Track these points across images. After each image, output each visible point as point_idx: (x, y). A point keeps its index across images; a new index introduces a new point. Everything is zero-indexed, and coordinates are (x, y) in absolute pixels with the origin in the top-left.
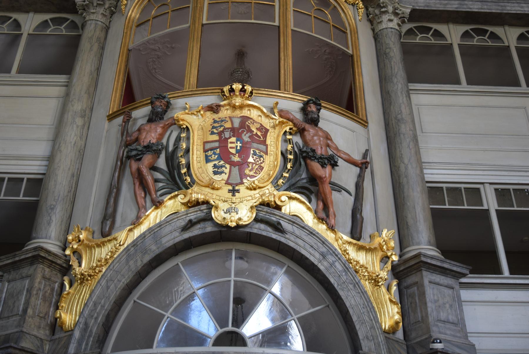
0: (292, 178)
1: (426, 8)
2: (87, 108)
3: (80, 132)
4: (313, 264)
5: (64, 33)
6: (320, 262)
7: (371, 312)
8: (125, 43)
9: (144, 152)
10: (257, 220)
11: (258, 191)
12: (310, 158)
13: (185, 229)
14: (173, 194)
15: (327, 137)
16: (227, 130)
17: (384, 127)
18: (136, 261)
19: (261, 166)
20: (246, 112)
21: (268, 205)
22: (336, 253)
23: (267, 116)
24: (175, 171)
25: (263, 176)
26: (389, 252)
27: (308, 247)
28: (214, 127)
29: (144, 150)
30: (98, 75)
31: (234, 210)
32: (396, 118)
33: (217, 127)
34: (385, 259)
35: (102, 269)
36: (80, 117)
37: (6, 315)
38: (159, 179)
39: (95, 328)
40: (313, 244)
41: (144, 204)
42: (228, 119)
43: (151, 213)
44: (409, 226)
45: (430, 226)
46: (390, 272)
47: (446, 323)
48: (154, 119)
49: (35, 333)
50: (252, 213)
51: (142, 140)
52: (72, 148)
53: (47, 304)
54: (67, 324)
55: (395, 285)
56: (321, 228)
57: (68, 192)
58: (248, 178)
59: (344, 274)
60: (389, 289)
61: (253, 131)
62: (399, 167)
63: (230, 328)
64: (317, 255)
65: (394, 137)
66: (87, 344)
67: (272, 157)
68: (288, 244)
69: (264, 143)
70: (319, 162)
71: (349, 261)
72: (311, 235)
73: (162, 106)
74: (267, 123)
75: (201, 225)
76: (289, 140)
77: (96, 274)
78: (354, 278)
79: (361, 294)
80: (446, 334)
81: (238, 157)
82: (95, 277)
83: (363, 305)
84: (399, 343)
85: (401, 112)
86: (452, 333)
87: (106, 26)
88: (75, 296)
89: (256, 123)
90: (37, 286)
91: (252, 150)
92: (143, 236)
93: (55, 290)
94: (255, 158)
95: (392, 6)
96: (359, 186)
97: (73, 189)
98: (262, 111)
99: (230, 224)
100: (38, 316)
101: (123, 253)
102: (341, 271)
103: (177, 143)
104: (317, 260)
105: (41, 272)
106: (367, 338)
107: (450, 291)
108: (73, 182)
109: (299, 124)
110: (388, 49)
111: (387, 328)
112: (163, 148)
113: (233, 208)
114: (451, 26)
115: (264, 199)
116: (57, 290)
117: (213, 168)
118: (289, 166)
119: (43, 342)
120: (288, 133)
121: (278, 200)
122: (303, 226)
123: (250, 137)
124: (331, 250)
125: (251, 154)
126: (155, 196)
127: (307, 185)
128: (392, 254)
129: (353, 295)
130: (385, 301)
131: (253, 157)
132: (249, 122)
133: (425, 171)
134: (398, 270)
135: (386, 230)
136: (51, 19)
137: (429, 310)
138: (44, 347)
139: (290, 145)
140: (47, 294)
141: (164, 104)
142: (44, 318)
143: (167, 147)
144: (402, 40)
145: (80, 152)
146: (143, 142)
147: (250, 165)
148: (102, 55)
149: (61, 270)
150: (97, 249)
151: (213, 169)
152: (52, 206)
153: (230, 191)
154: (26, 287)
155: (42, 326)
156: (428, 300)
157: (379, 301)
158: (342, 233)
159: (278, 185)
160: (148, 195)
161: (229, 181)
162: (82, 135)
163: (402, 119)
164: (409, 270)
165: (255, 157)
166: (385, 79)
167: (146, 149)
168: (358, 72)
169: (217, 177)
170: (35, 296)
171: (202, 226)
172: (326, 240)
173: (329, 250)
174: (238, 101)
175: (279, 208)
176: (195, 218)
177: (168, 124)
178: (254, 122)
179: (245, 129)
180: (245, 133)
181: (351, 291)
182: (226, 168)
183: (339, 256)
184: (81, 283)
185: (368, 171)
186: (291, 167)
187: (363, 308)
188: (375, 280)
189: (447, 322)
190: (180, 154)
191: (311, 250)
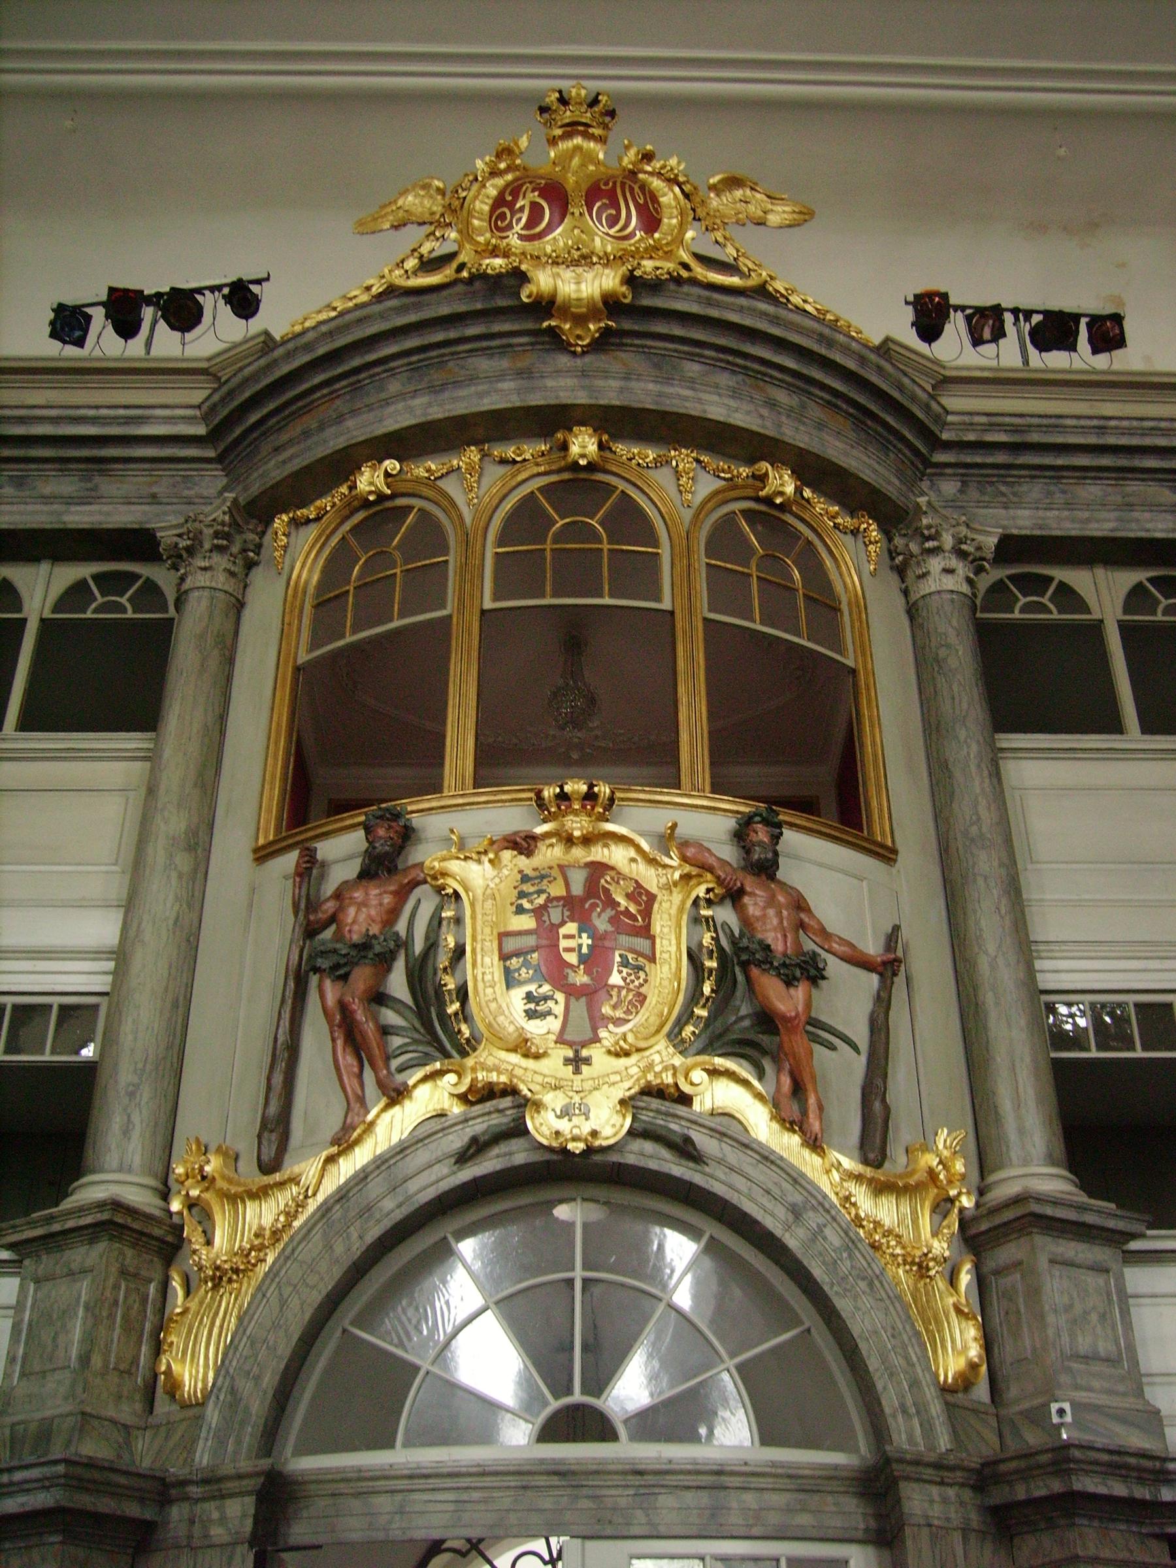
0: (715, 1018)
1: (1038, 532)
3: (187, 888)
4: (771, 1235)
5: (130, 614)
6: (788, 1228)
8: (288, 654)
9: (356, 960)
10: (631, 1133)
11: (634, 1058)
12: (758, 964)
13: (463, 1157)
14: (428, 1069)
15: (800, 905)
16: (555, 903)
17: (936, 854)
18: (348, 1237)
19: (639, 994)
20: (599, 853)
22: (827, 1206)
23: (652, 862)
24: (433, 1009)
27: (758, 1193)
29: (354, 953)
30: (222, 733)
32: (966, 833)
33: (531, 894)
34: (943, 1206)
35: (266, 1254)
36: (186, 849)
37: (37, 1368)
38: (392, 1027)
39: (257, 1405)
40: (771, 1186)
41: (360, 1092)
42: (555, 872)
43: (378, 1116)
46: (955, 1239)
49: (111, 1412)
50: (624, 1116)
51: (347, 928)
54: (187, 1389)
55: (968, 1272)
56: (788, 1145)
58: (611, 1026)
59: (845, 1255)
60: (953, 1281)
61: (619, 904)
63: (577, 1397)
64: (781, 1212)
65: (963, 884)
66: (239, 1442)
67: (666, 968)
68: (711, 1189)
69: (645, 932)
70: (779, 975)
71: (858, 1221)
73: (391, 839)
74: (650, 878)
76: (707, 919)
79: (888, 1302)
80: (1089, 1389)
82: (250, 1274)
83: (893, 1328)
85: (979, 819)
86: (1106, 1385)
87: (238, 600)
88: (202, 1318)
92: (362, 1177)
94: (624, 974)
95: (951, 532)
96: (879, 1027)
97: (177, 1041)
99: (570, 1146)
100: (114, 1369)
101: (317, 1217)
103: (432, 935)
106: (905, 1411)
107: (1100, 1280)
110: (944, 649)
111: (950, 1380)
112: (398, 946)
114: (1100, 572)
116: (154, 1300)
118: (707, 989)
119: (129, 1433)
120: (702, 903)
121: (683, 1080)
122: (746, 1141)
123: (613, 920)
126: (385, 1072)
127: (751, 1036)
128: (960, 1194)
131: (620, 972)
132: (608, 879)
133: (1038, 964)
134: (973, 1231)
135: (945, 1131)
136: (97, 578)
140: (133, 1313)
141: (396, 832)
142: (129, 1373)
143: (405, 944)
144: (979, 615)
145: (188, 941)
146: (350, 931)
147: (614, 993)
148: (229, 679)
150: (248, 1203)
154: (83, 1298)
155: (125, 1393)
157: (930, 1313)
159: (683, 1041)
161: (567, 1037)
165: (625, 970)
166: (938, 730)
168: (870, 717)
169: (535, 1028)
170: (105, 1321)
172: (803, 1175)
174: (577, 825)
175: (685, 1100)
176: (484, 1133)
178: (619, 876)
179: (599, 898)
183: (833, 1213)
184: (215, 1287)
185: (900, 980)
186: (713, 991)
188: (920, 1265)
189: (1093, 1359)
190: (443, 961)
191: (765, 1200)
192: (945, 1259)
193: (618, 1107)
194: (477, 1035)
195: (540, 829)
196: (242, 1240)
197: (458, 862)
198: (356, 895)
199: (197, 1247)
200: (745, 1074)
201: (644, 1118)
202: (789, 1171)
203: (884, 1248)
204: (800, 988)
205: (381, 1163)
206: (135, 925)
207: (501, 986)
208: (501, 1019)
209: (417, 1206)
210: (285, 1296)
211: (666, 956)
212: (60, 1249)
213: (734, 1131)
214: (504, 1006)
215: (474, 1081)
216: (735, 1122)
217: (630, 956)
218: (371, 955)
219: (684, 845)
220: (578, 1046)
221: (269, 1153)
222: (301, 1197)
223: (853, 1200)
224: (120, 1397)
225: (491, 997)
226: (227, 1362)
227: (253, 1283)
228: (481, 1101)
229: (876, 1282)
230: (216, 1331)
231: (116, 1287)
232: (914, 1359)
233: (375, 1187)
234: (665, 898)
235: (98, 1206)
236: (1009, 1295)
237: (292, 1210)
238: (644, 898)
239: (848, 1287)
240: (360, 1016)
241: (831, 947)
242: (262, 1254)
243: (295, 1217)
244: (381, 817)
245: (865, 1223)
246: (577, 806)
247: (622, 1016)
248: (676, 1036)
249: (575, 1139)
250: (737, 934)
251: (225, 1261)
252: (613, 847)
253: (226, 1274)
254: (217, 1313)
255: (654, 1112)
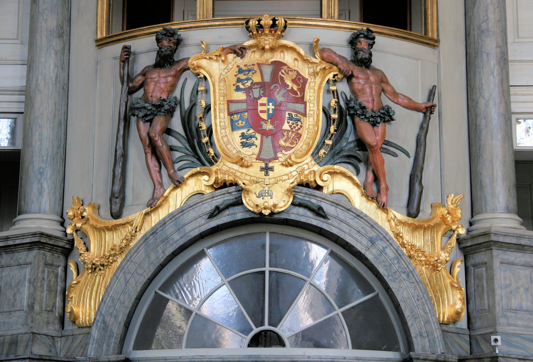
2: (64, 21)
7: (427, 304)
9: (155, 113)
10: (293, 204)
11: (295, 167)
12: (359, 116)
13: (212, 215)
15: (383, 80)
16: (256, 86)
18: (157, 252)
20: (278, 57)
21: (307, 185)
22: (388, 238)
23: (306, 61)
24: (195, 140)
25: (301, 147)
26: (454, 225)
27: (354, 233)
28: (239, 80)
29: (154, 109)
31: (268, 194)
32: (479, 27)
34: (449, 232)
36: (58, 37)
37: (6, 309)
39: (117, 330)
40: (360, 229)
41: (160, 181)
42: (256, 68)
43: (170, 193)
44: (483, 186)
45: (510, 187)
47: (518, 312)
48: (162, 64)
49: (45, 331)
50: (289, 197)
51: (150, 95)
52: (54, 85)
53: (53, 294)
54: (81, 319)
55: (458, 267)
57: (58, 147)
58: (283, 151)
59: (396, 261)
61: (288, 86)
62: (477, 103)
63: (266, 327)
64: (365, 241)
66: (108, 346)
67: (311, 119)
68: (331, 231)
69: (302, 100)
70: (369, 121)
72: (358, 218)
74: (305, 71)
75: (231, 210)
77: (110, 264)
78: (407, 266)
79: (416, 283)
80: (516, 326)
81: (270, 124)
83: (418, 296)
84: (461, 335)
85: (487, 19)
86: (525, 323)
88: (87, 287)
89: (291, 71)
90: (40, 276)
91: (287, 113)
92: (163, 223)
93: (59, 275)
94: (290, 124)
98: (299, 54)
100: (45, 310)
101: (141, 242)
102: (393, 258)
104: (364, 248)
105: (43, 259)
106: (421, 335)
108: (61, 133)
109: (345, 70)
111: (446, 320)
112: (176, 104)
113: (267, 191)
115: (302, 180)
117: (241, 138)
118: (332, 129)
120: (331, 83)
121: (318, 178)
122: (349, 208)
124: (382, 234)
125: (286, 119)
126: (172, 171)
128: (458, 227)
129: (406, 286)
130: (445, 286)
131: (288, 123)
132: (283, 71)
133: (513, 98)
134: (463, 245)
135: (453, 195)
137: (497, 298)
138: (56, 344)
139: (335, 100)
140: (52, 283)
141: (173, 43)
142: (52, 311)
143: (180, 103)
149: (64, 251)
151: (241, 139)
152: (41, 170)
153: (262, 169)
154: (28, 277)
155: (51, 321)
156: (496, 286)
157: (437, 288)
158: (396, 211)
159: (319, 157)
160: (163, 167)
161: (261, 157)
162: (64, 63)
163: (488, 29)
164: (477, 246)
165: (291, 122)
167: (157, 108)
169: (246, 152)
170: (39, 289)
171: (231, 212)
172: (376, 224)
173: (379, 234)
174: (268, 41)
175: (319, 188)
176: (222, 204)
177: (180, 70)
178: (290, 69)
179: (278, 83)
180: (278, 90)
181: (404, 281)
182: (257, 139)
183: (391, 241)
185: (434, 117)
186: (335, 131)
187: (418, 300)
188: (433, 265)
190: (199, 113)
191: (357, 236)
192: (447, 262)
193: (287, 192)
194: (217, 154)
195: (247, 43)
196: (104, 251)
197: (205, 60)
198: (154, 76)
199: (82, 252)
200: (350, 173)
201: (300, 197)
202: (370, 221)
203: (416, 257)
204: (380, 127)
205: (172, 217)
206: (34, 80)
207: (229, 129)
208: (229, 146)
209: (190, 238)
210: (128, 278)
211: (311, 112)
212: (13, 252)
213: (343, 202)
214: (231, 139)
215: (217, 178)
216: (344, 197)
217: (293, 114)
218: (163, 110)
219: (322, 51)
220: (267, 161)
221: (116, 208)
222: (134, 232)
223: (401, 235)
224: (48, 323)
225: (224, 135)
226: (101, 309)
227: (111, 271)
228: (221, 188)
229: (411, 274)
230: (94, 293)
231: (43, 272)
232: (428, 310)
233: (170, 229)
234: (312, 80)
235: (32, 235)
236: (479, 277)
237: (129, 238)
238: (301, 81)
239: (397, 277)
240: (159, 143)
241: (398, 101)
242: (115, 258)
243: (131, 241)
244: (165, 35)
245: (406, 246)
246: (267, 32)
247: (289, 145)
248: (316, 154)
249: (265, 208)
250: (349, 98)
251: (97, 261)
252: (286, 53)
253: (98, 267)
254: (94, 284)
255: (303, 195)
